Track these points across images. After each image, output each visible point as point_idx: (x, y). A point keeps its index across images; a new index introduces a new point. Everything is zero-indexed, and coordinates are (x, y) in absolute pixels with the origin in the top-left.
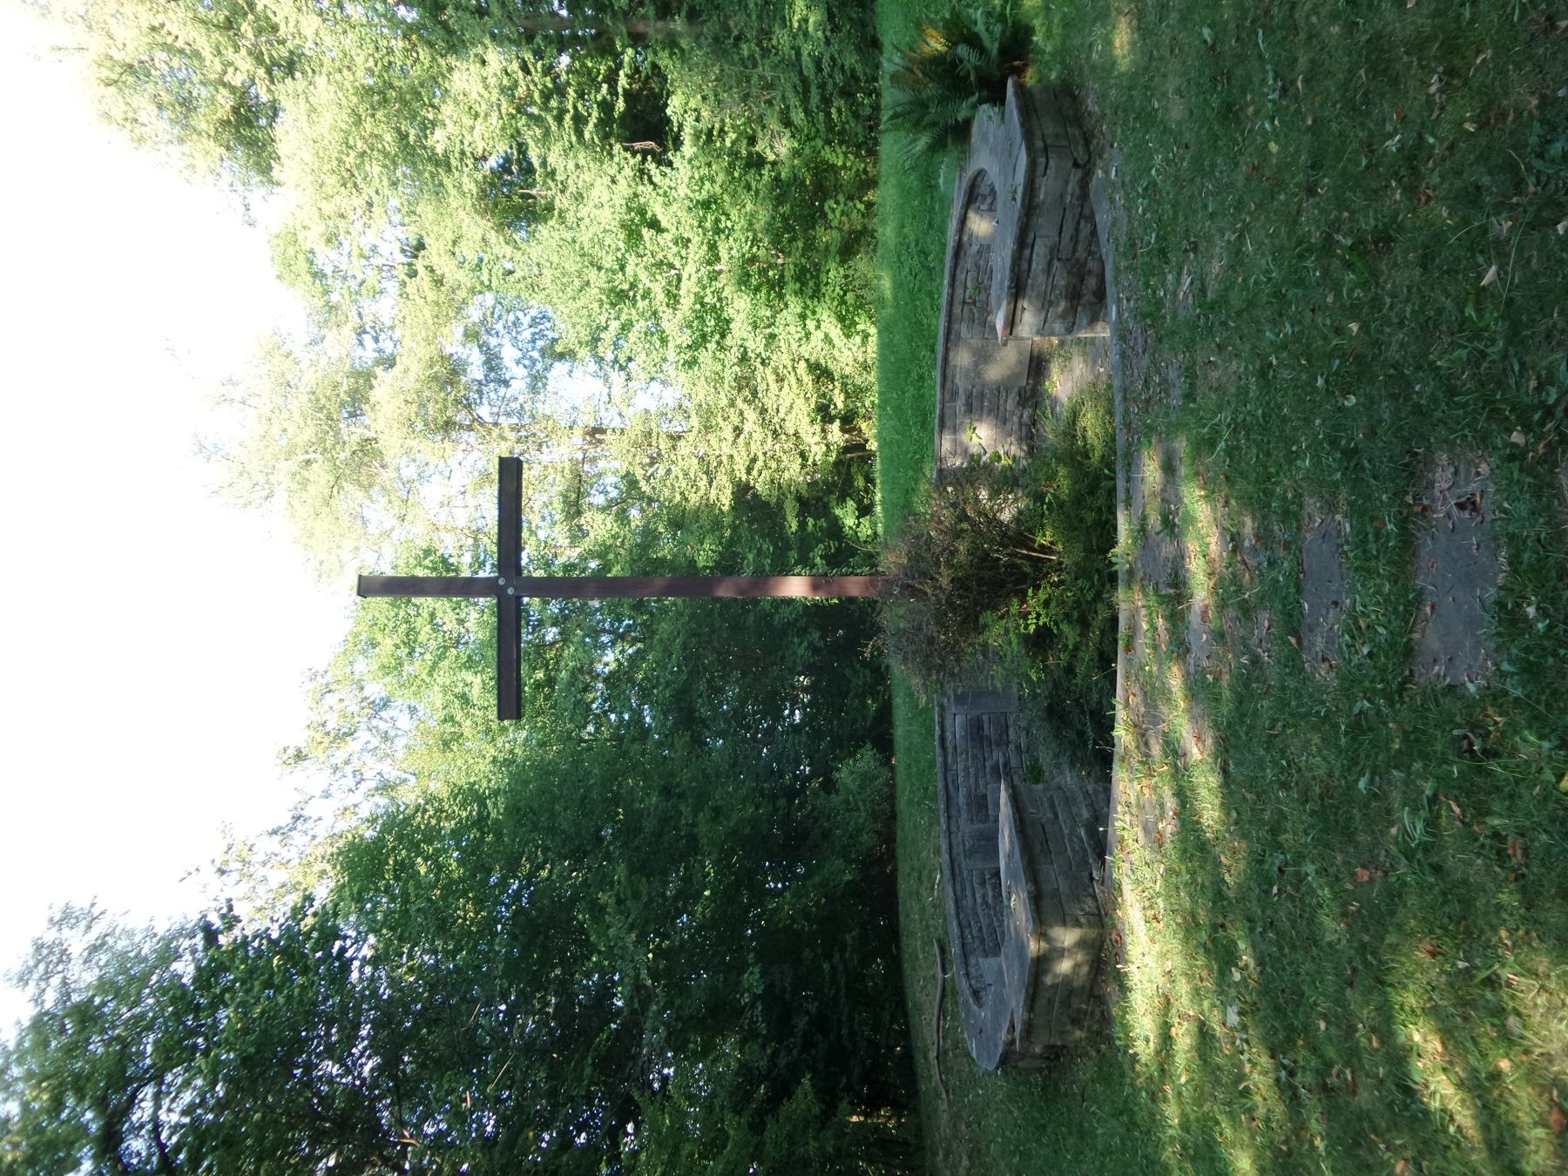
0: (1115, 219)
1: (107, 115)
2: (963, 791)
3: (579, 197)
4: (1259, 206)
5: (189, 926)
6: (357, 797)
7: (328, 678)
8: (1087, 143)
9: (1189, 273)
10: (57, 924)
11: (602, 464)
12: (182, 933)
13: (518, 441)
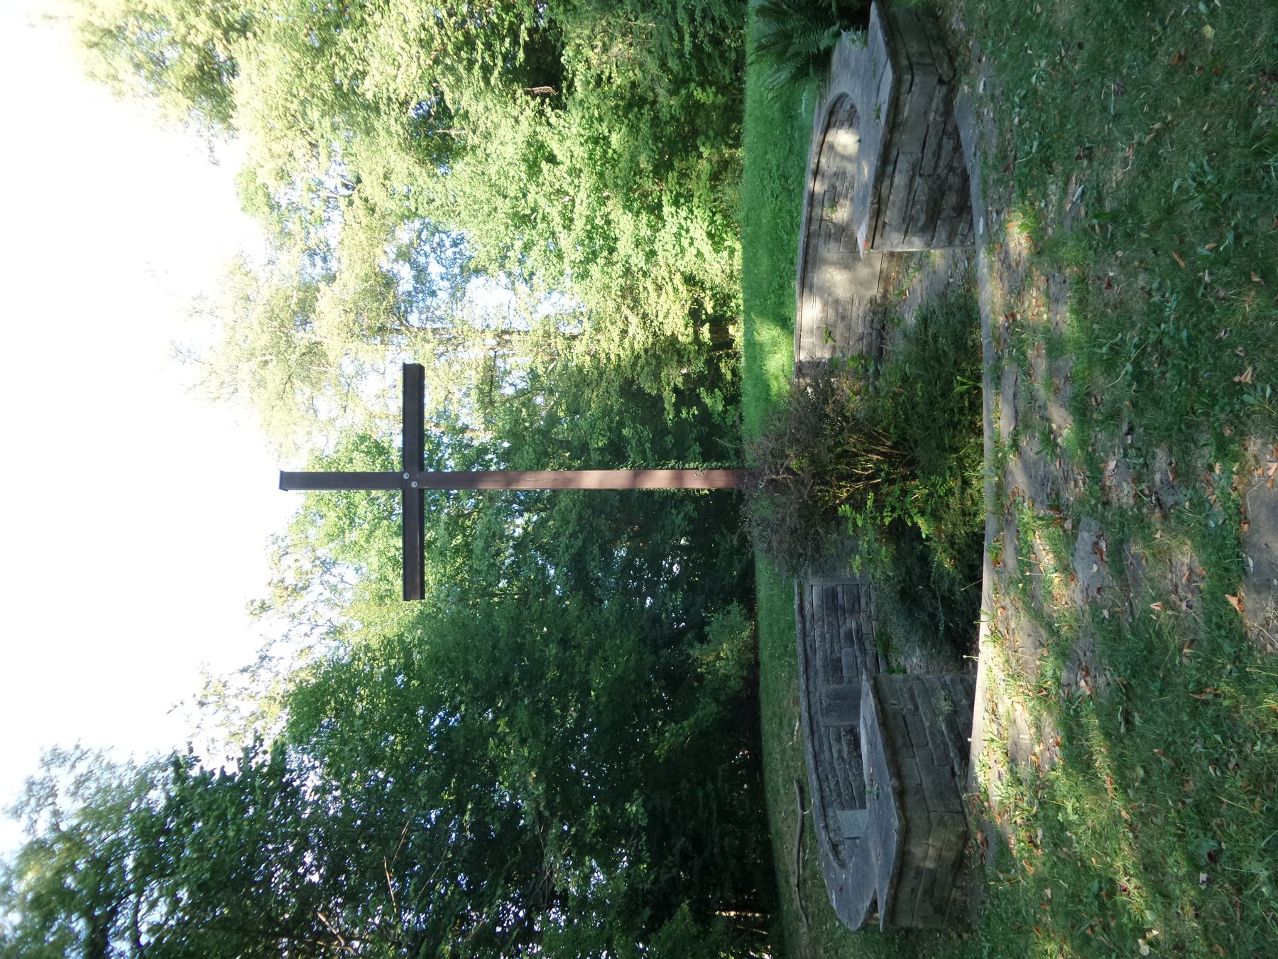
0: (982, 134)
1: (93, 75)
2: (819, 655)
3: (487, 136)
4: (1188, 101)
5: (162, 761)
6: (312, 640)
7: (288, 541)
8: (951, 60)
9: (1079, 182)
10: (46, 764)
11: (511, 361)
12: (157, 766)
13: (441, 342)
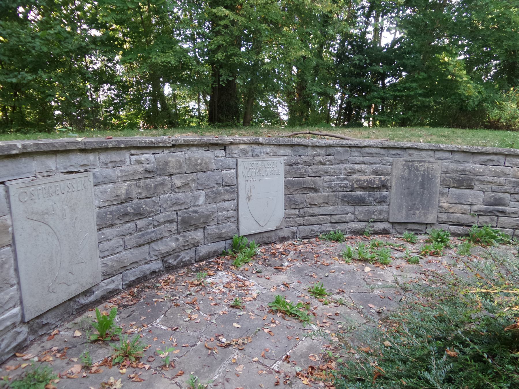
2: (479, 168)
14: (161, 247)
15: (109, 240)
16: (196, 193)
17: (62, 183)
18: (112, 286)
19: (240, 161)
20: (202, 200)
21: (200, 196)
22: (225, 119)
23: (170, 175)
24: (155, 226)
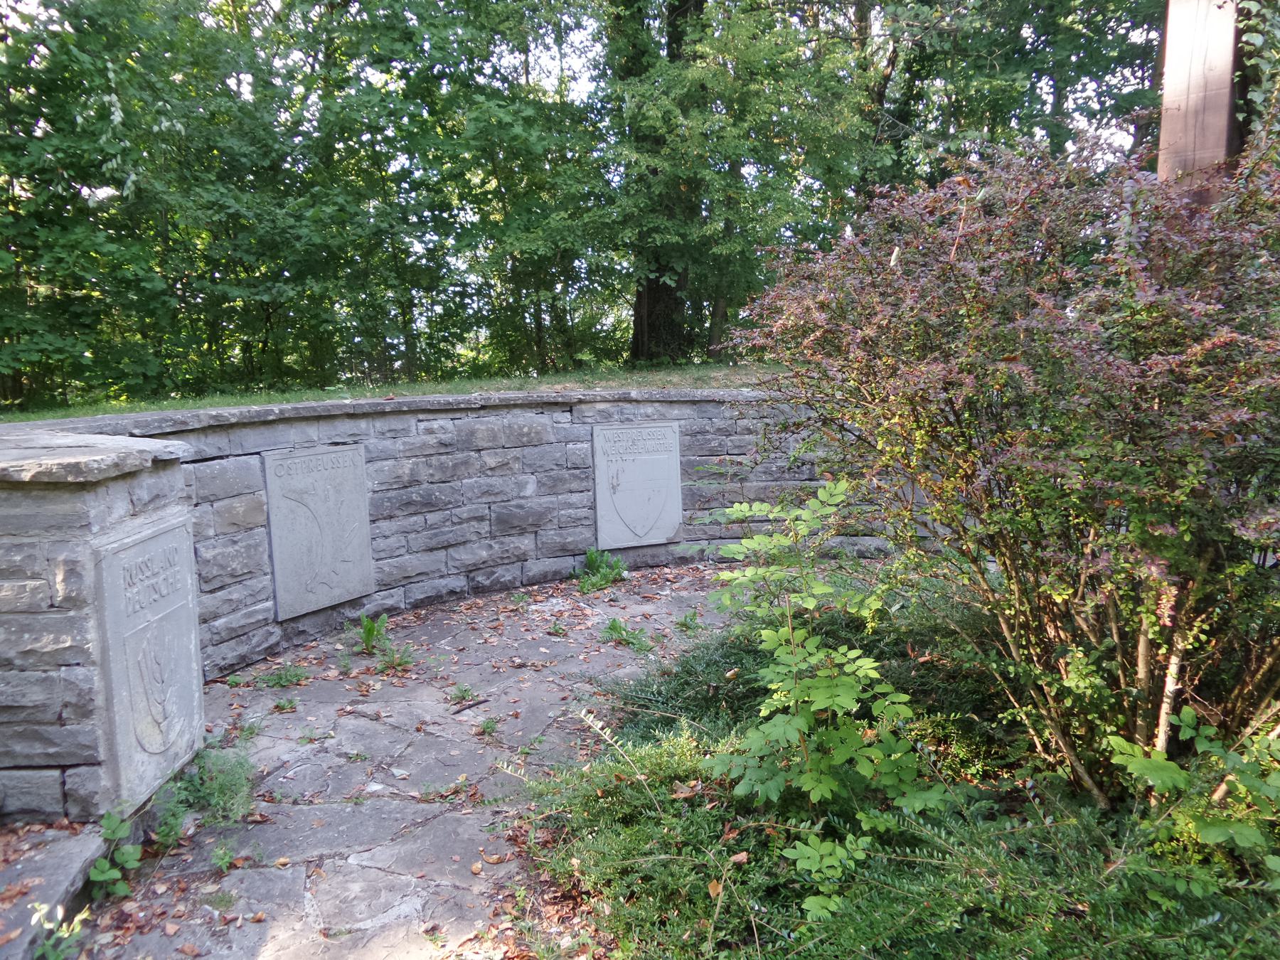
14: (464, 556)
15: (386, 537)
16: (522, 478)
17: (325, 457)
18: (390, 602)
19: (597, 429)
20: (530, 489)
21: (527, 483)
22: (661, 350)
23: (479, 451)
24: (454, 524)
